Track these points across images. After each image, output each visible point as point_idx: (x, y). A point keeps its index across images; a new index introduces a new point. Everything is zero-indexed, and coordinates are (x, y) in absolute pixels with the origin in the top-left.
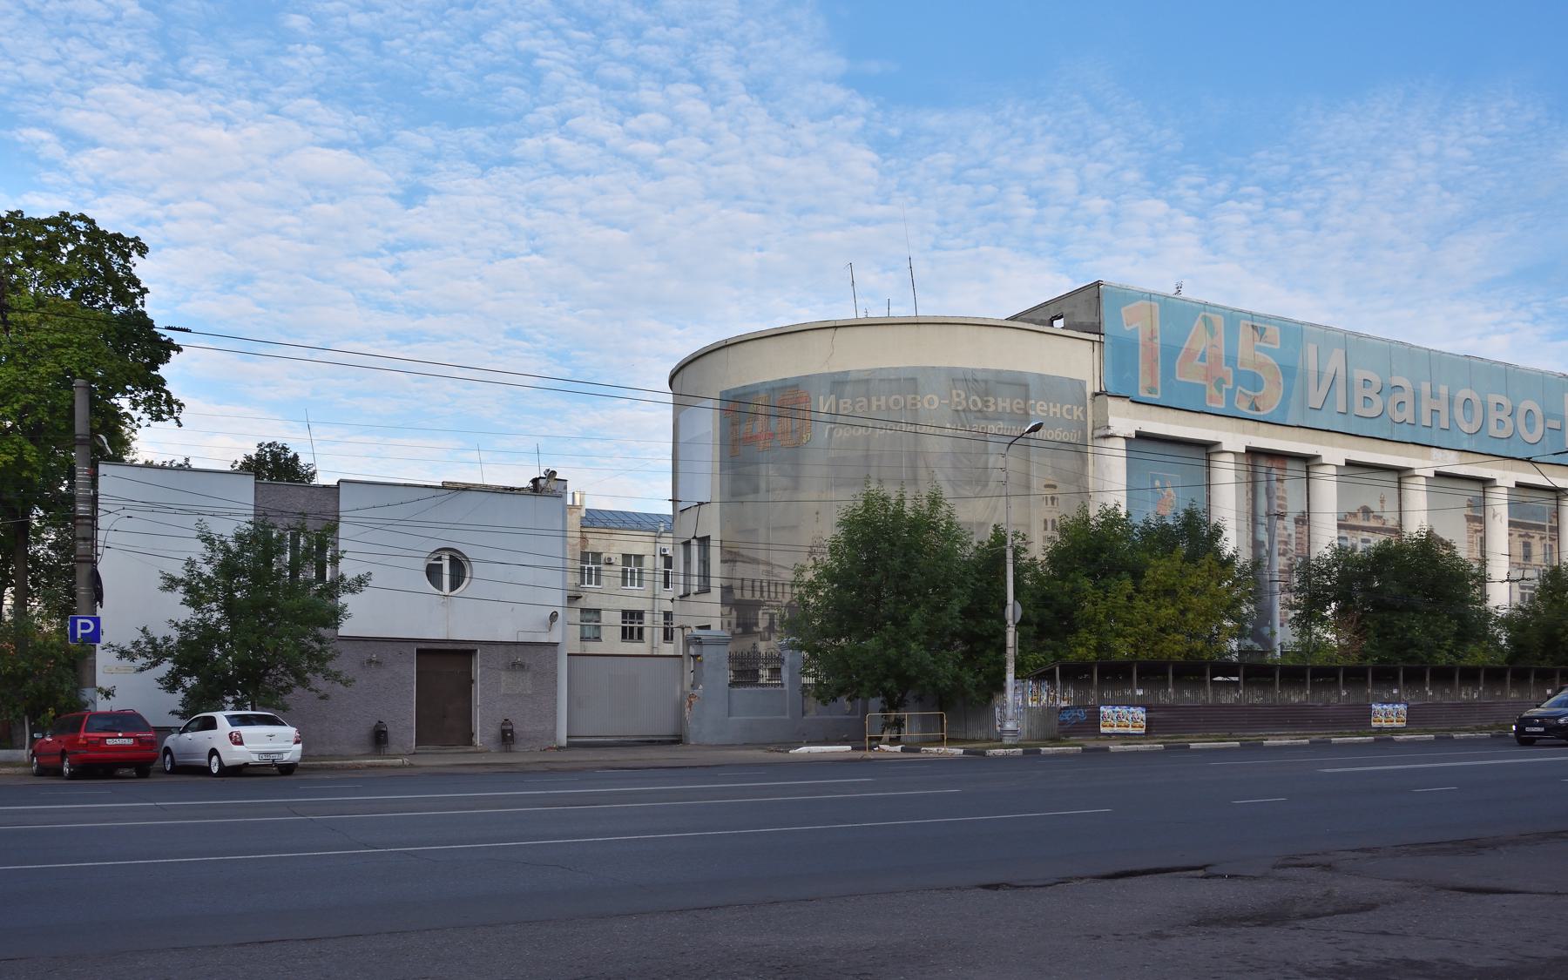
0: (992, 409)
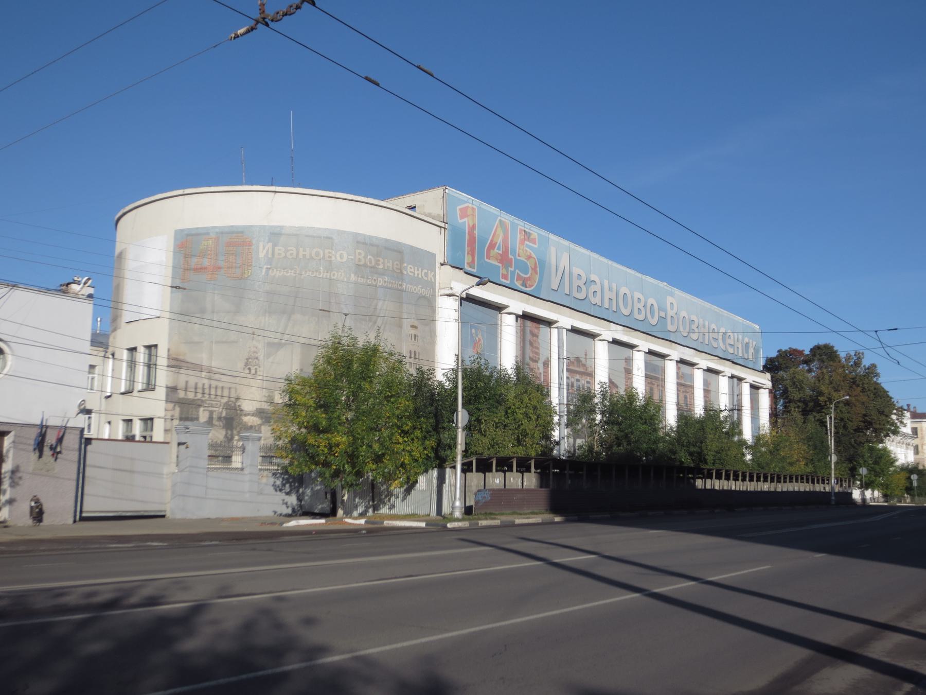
0: (381, 267)
